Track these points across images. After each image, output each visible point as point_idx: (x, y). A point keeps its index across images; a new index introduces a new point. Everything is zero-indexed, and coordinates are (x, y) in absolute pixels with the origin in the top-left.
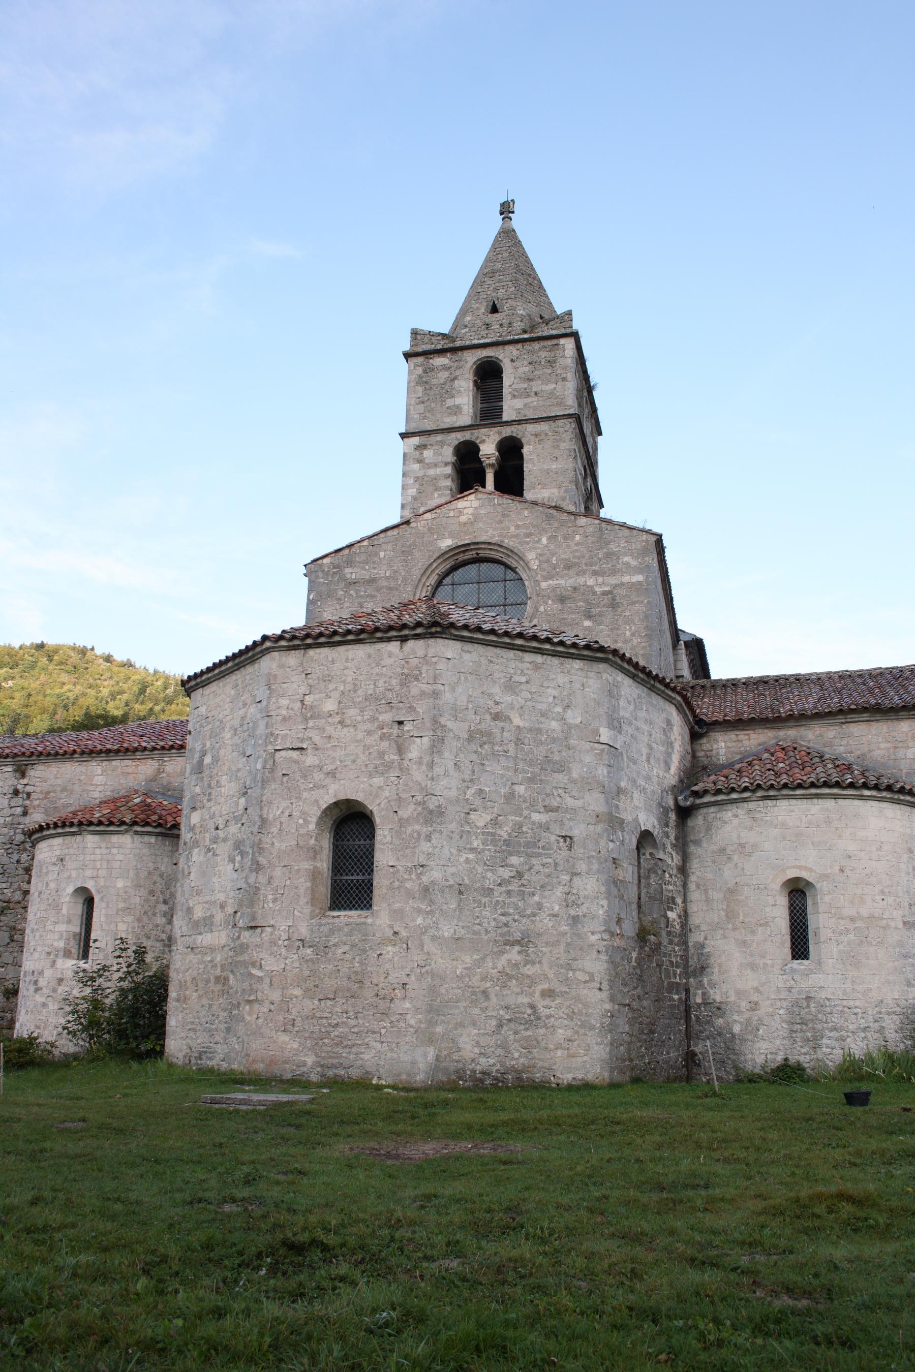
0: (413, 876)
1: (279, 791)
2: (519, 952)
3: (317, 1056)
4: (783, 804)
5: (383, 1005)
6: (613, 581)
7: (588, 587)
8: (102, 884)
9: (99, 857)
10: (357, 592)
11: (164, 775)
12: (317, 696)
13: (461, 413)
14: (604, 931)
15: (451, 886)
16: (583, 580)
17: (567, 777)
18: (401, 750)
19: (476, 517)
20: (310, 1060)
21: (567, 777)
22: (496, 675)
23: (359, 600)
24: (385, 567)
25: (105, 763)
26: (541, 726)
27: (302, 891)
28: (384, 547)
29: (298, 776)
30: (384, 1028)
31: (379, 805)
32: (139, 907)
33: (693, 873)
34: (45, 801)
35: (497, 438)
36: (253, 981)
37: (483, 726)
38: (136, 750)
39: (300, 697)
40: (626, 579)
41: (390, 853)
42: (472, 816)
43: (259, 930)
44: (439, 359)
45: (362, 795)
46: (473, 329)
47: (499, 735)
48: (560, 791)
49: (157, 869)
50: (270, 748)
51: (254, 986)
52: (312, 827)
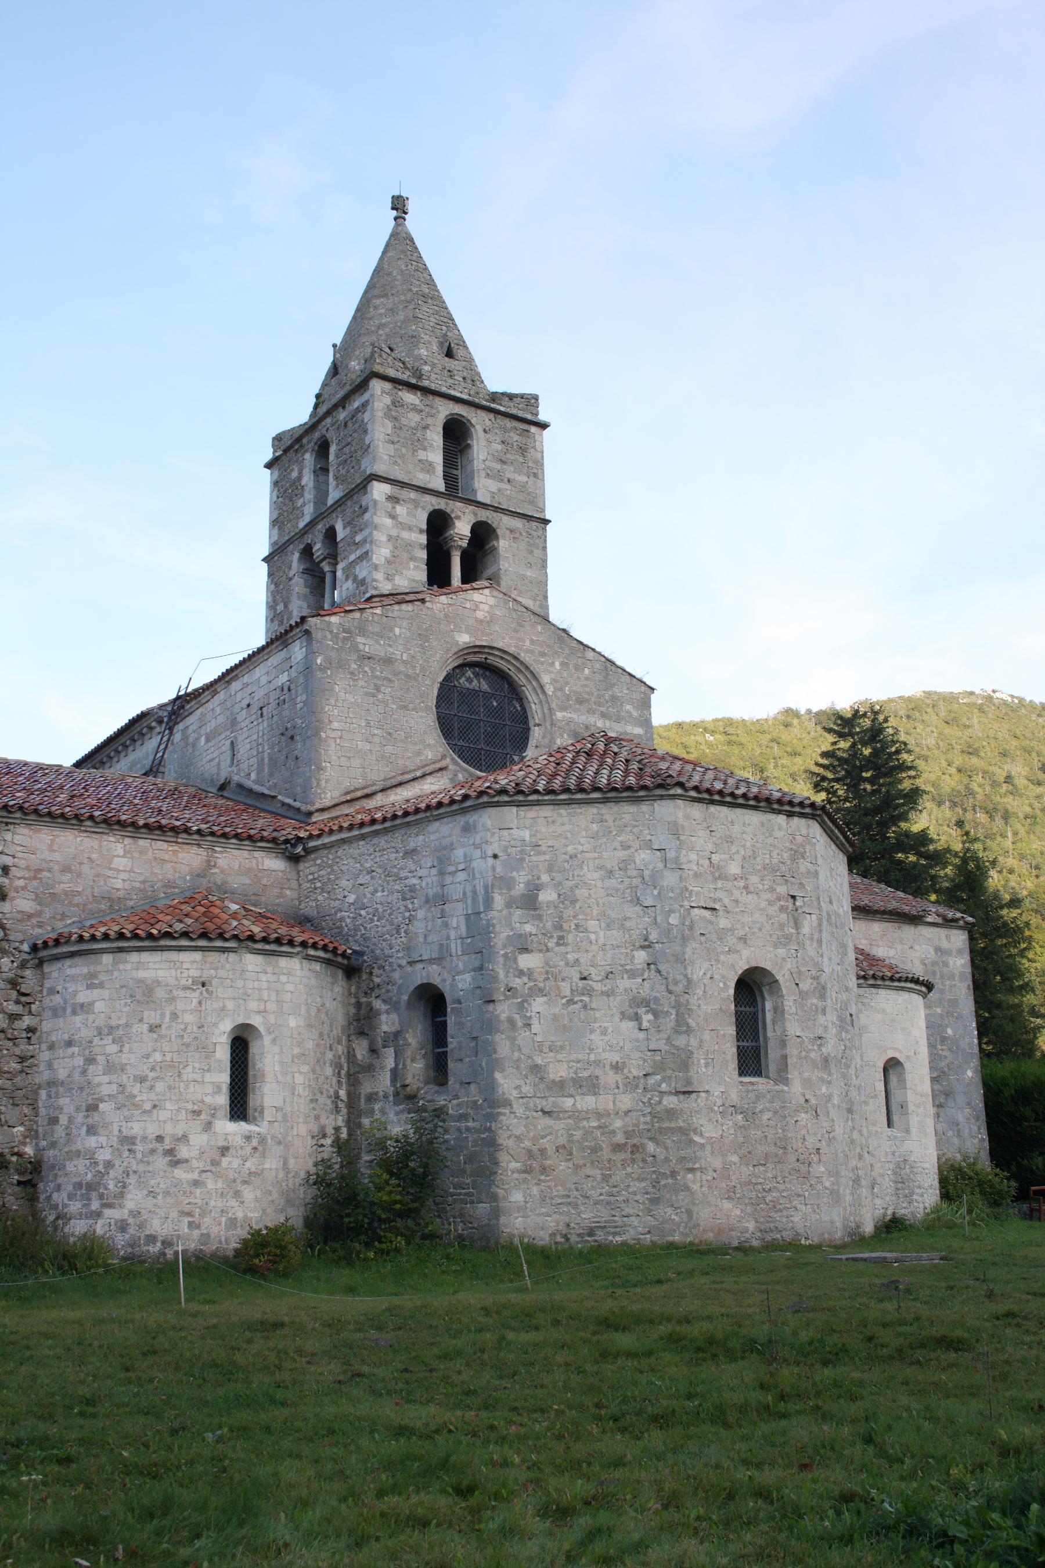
0: (815, 1047)
1: (699, 951)
3: (757, 1222)
4: (882, 992)
5: (804, 1169)
8: (272, 1021)
9: (265, 985)
10: (373, 670)
11: (217, 870)
12: (723, 857)
18: (797, 926)
20: (751, 1226)
23: (375, 681)
24: (401, 648)
25: (127, 841)
28: (399, 622)
29: (714, 937)
32: (313, 1054)
34: (35, 883)
38: (174, 830)
39: (707, 853)
44: (408, 395)
49: (323, 1005)
51: (698, 1154)
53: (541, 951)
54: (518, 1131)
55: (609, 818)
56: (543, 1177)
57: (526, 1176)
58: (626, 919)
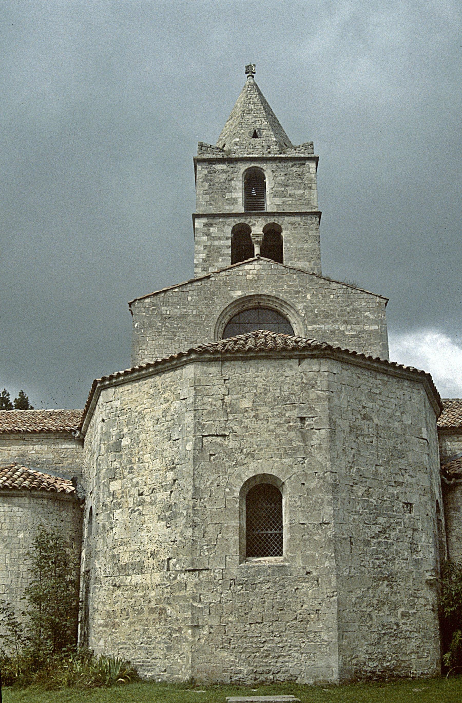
2: (387, 585)
5: (301, 626)
6: (358, 328)
7: (341, 331)
12: (234, 397)
13: (236, 203)
14: (433, 570)
15: (345, 539)
16: (337, 326)
17: (406, 462)
18: (304, 438)
19: (259, 277)
20: (245, 669)
21: (406, 462)
22: (362, 387)
23: (173, 330)
26: (390, 425)
27: (231, 543)
30: (304, 642)
31: (290, 478)
33: (453, 530)
35: (264, 224)
36: (194, 612)
37: (357, 423)
39: (221, 396)
40: (367, 327)
41: (301, 514)
42: (354, 488)
43: (197, 572)
45: (276, 470)
46: (242, 147)
47: (367, 430)
48: (403, 471)
50: (199, 434)
52: (237, 494)
53: (120, 478)
54: (103, 599)
55: (159, 383)
56: (114, 630)
57: (105, 628)
58: (164, 450)
